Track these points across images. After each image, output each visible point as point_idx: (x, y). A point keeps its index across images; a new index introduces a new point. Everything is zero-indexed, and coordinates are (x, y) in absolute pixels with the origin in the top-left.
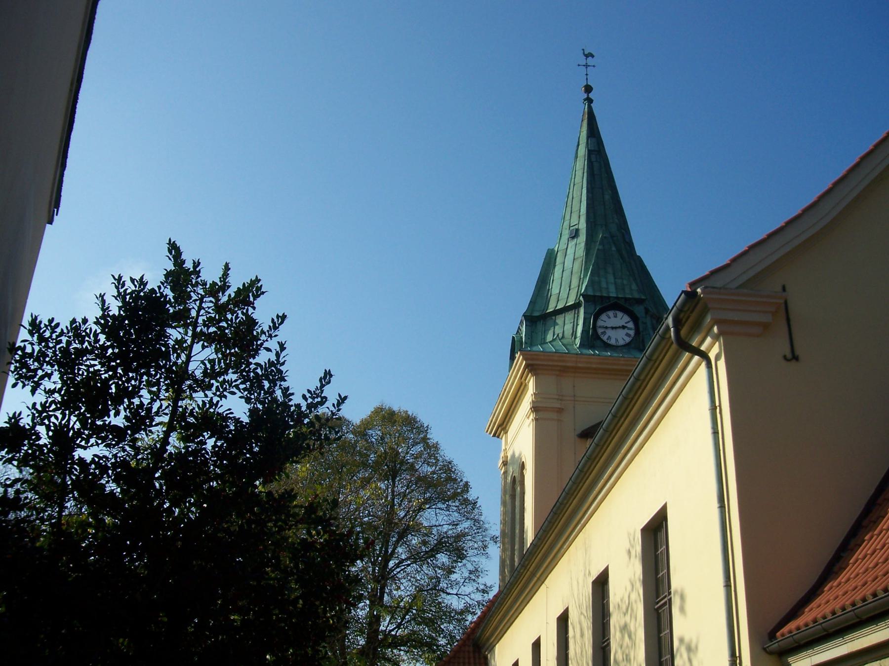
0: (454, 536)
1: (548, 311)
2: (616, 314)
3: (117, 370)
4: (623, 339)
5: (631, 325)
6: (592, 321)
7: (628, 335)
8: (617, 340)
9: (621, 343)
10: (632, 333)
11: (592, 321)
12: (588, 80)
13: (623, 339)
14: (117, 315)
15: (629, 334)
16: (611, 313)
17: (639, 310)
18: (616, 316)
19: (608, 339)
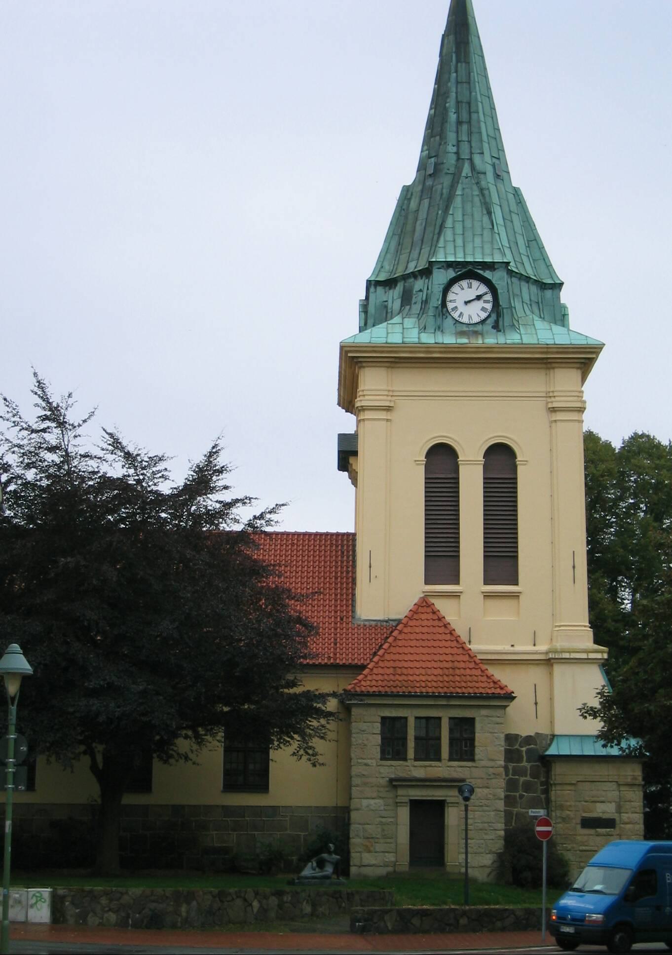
0: (232, 925)
1: (548, 753)
2: (471, 283)
3: (631, 606)
4: (478, 315)
5: (489, 297)
6: (662, 854)
7: (483, 309)
8: (470, 317)
9: (476, 320)
10: (489, 306)
11: (662, 854)
12: (538, 705)
13: (478, 315)
14: (617, 451)
15: (483, 311)
16: (464, 283)
17: (497, 277)
18: (470, 287)
19: (459, 316)
